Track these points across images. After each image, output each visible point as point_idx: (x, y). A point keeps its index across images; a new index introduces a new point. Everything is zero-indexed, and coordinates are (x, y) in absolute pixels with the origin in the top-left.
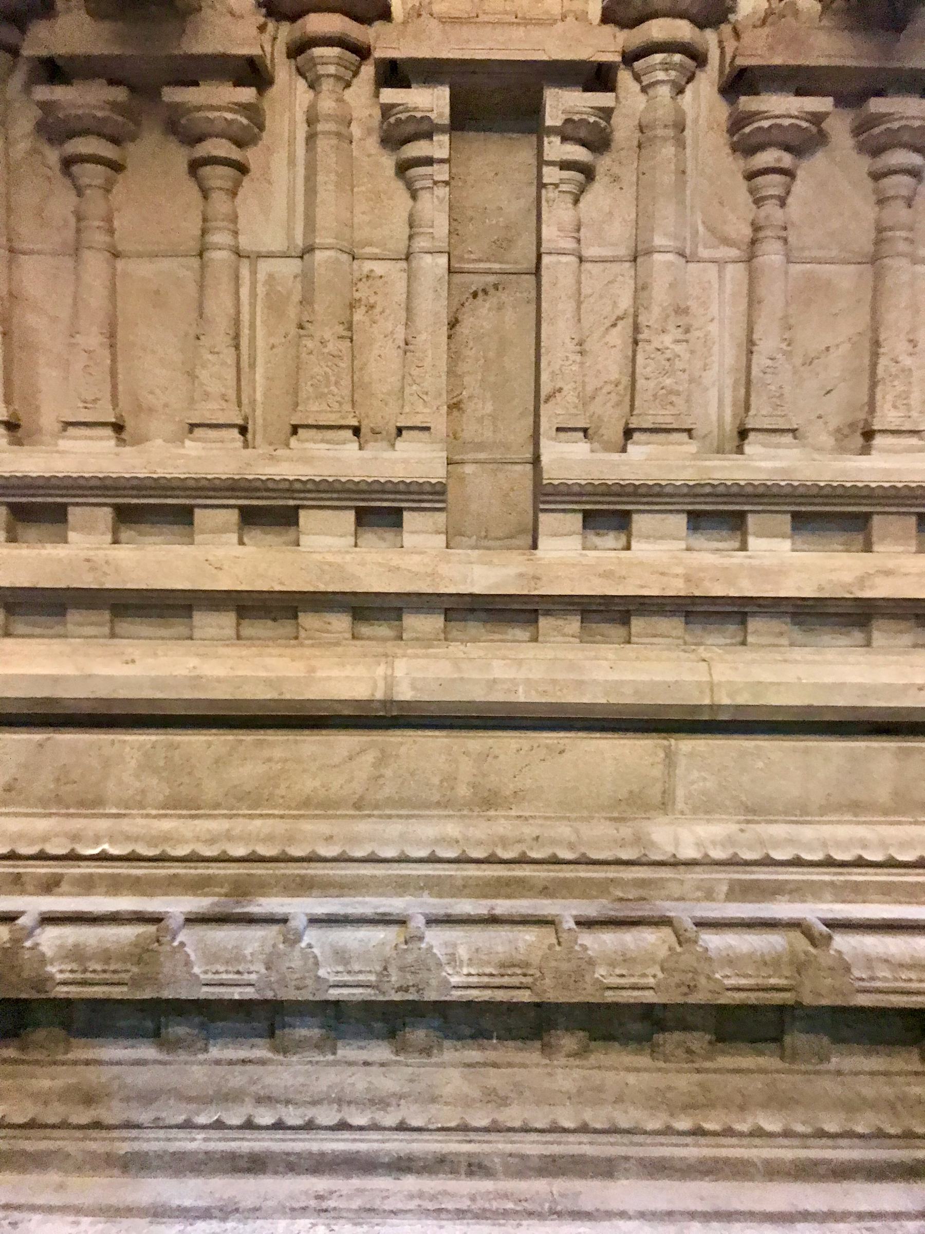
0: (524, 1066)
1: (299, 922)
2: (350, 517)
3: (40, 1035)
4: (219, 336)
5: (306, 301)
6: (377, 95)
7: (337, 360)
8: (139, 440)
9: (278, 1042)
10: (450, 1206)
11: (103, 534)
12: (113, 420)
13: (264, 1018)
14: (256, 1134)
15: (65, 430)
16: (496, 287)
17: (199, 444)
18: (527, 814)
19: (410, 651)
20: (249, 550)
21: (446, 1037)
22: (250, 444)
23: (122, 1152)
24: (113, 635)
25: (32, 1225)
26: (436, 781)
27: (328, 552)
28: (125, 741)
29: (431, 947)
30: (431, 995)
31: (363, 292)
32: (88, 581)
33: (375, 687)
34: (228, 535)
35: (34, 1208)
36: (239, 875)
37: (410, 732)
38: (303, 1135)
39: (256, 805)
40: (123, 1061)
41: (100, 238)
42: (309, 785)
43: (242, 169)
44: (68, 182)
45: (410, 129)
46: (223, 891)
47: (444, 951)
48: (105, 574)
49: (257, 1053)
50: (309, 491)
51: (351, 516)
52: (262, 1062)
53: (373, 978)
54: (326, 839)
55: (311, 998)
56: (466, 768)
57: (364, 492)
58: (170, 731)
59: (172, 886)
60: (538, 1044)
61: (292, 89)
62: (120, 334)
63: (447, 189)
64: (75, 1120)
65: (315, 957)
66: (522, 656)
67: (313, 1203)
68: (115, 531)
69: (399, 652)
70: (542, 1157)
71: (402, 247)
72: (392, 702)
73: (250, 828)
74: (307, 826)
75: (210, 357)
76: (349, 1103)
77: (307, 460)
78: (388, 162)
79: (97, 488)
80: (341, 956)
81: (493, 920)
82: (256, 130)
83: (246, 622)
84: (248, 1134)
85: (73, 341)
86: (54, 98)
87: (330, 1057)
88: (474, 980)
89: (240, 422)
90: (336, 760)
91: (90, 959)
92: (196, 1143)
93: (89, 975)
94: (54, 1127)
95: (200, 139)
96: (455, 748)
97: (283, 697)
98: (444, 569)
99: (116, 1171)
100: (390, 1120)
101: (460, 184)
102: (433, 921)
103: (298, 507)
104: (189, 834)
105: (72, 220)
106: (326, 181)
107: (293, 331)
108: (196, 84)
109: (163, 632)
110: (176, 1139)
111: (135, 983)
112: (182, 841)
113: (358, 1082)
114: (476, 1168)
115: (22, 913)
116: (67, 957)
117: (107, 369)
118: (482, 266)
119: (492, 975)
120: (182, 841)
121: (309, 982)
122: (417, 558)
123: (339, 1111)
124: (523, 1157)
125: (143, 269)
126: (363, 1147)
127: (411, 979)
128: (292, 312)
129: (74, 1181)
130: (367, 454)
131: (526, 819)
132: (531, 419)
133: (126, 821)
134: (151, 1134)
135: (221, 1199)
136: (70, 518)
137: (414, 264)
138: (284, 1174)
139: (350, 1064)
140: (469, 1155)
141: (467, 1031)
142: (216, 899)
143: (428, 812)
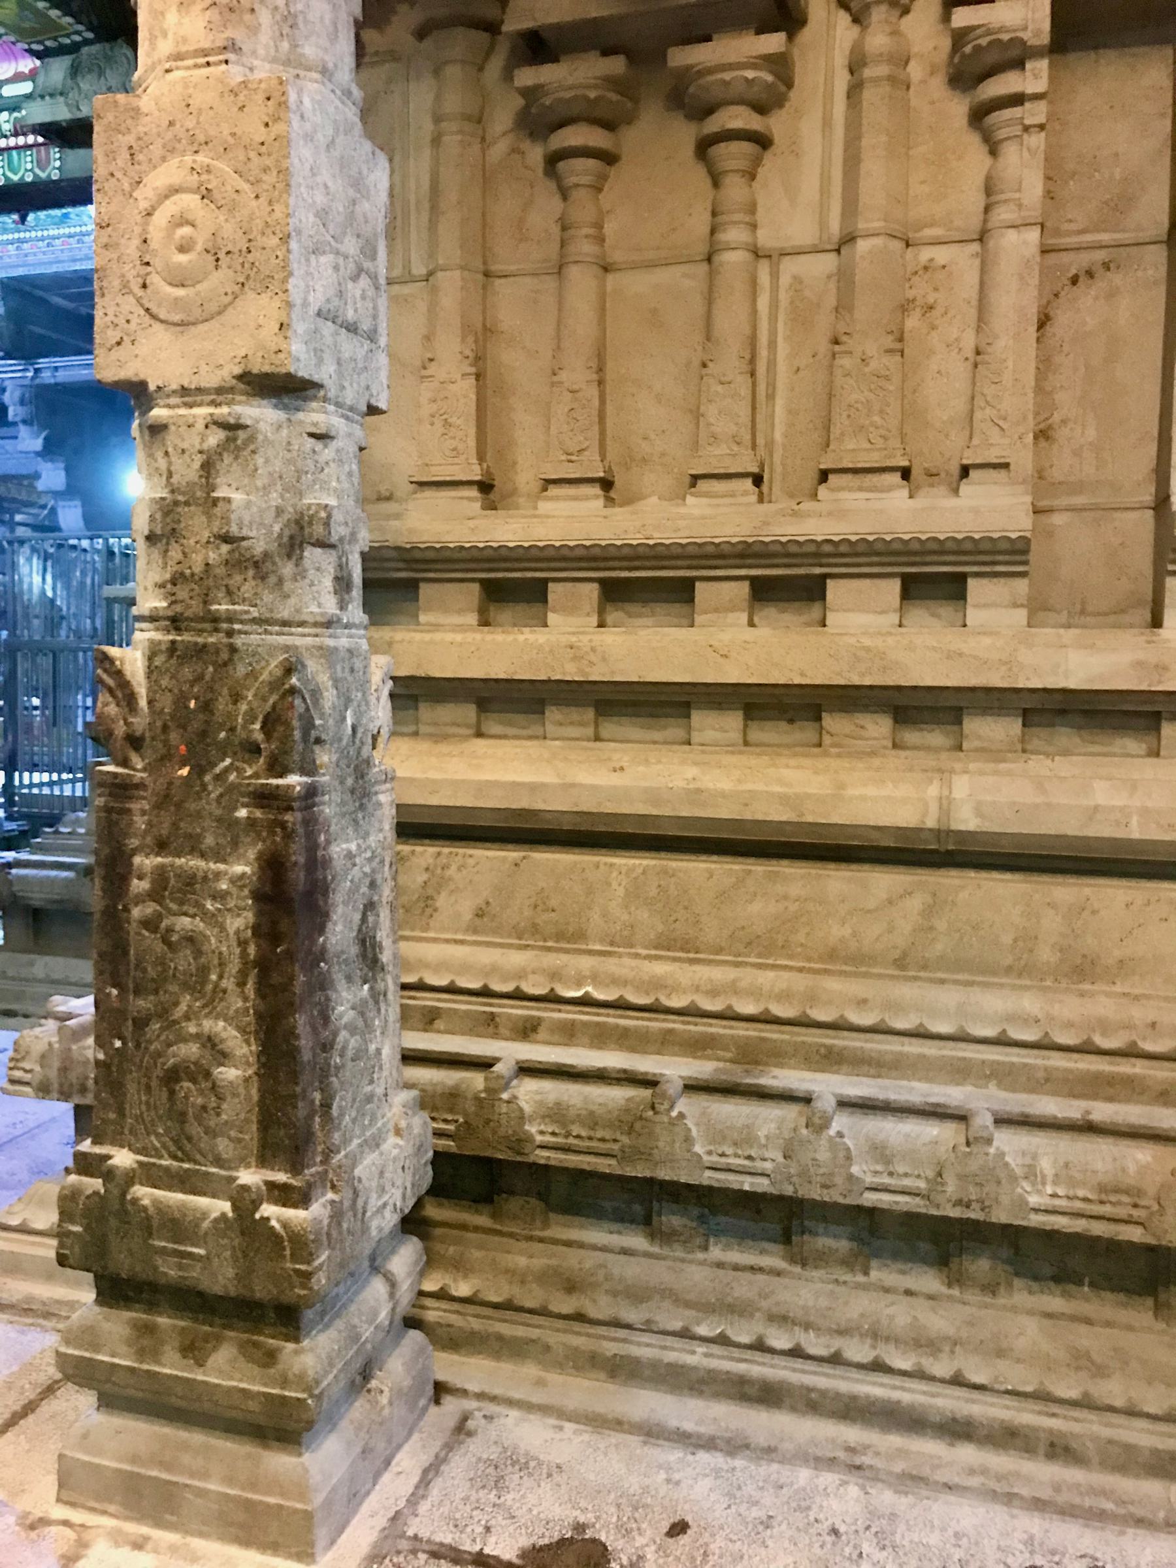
0: (1130, 1328)
1: (826, 1103)
2: (894, 587)
3: (514, 1204)
4: (730, 363)
5: (843, 307)
6: (946, 18)
7: (882, 382)
8: (628, 501)
9: (795, 1250)
10: (1025, 1492)
11: (588, 615)
12: (602, 474)
13: (781, 1218)
14: (767, 1358)
15: (546, 490)
16: (1106, 266)
17: (704, 500)
18: (1137, 991)
19: (972, 766)
20: (763, 633)
21: (1017, 1274)
22: (766, 499)
23: (609, 1354)
24: (597, 738)
25: (510, 1421)
26: (1007, 939)
27: (865, 634)
28: (612, 865)
29: (1003, 1154)
30: (1001, 1216)
31: (920, 290)
32: (570, 672)
33: (925, 814)
34: (737, 614)
35: (510, 1403)
36: (748, 1038)
37: (972, 874)
38: (827, 1369)
39: (768, 951)
40: (606, 1248)
41: (587, 248)
42: (837, 932)
43: (763, 141)
44: (553, 185)
45: (991, 58)
46: (729, 1055)
47: (1020, 1161)
48: (592, 663)
49: (766, 1261)
50: (843, 555)
51: (895, 586)
52: (779, 1273)
53: (922, 1184)
54: (858, 1003)
55: (841, 1200)
56: (1051, 924)
57: (915, 553)
58: (663, 855)
59: (665, 1043)
60: (1150, 1302)
61: (831, 26)
62: (610, 365)
63: (1043, 134)
64: (554, 1308)
65: (848, 1149)
66: (1136, 776)
67: (841, 1455)
68: (601, 612)
69: (958, 766)
70: (1155, 1452)
71: (975, 223)
72: (949, 832)
73: (760, 980)
74: (833, 985)
75: (720, 388)
76: (887, 1339)
77: (839, 514)
78: (958, 108)
79: (580, 559)
80: (881, 1152)
81: (1089, 1128)
82: (783, 88)
83: (754, 725)
84: (758, 1356)
85: (555, 379)
86: (542, 80)
87: (861, 1278)
88: (1061, 1203)
89: (755, 470)
90: (871, 904)
91: (573, 1123)
92: (697, 1357)
93: (571, 1141)
94: (531, 1311)
95: (709, 111)
96: (1037, 896)
97: (803, 820)
98: (1026, 656)
99: (602, 1375)
100: (941, 1368)
101: (1058, 127)
102: (1002, 1121)
103: (825, 577)
104: (686, 981)
105: (556, 230)
106: (872, 142)
107: (824, 347)
108: (708, 39)
109: (657, 735)
110: (673, 1349)
111: (623, 1157)
112: (675, 989)
113: (900, 1315)
114: (1059, 1450)
115: (498, 1060)
116: (549, 1116)
117: (595, 413)
118: (1089, 238)
119: (1086, 1200)
120: (675, 989)
121: (839, 1180)
122: (990, 640)
123: (874, 1347)
124: (1129, 1448)
125: (636, 284)
126: (906, 1398)
127: (973, 1193)
128: (824, 323)
129: (554, 1378)
130: (919, 502)
131: (1137, 998)
132: (1153, 449)
133: (612, 960)
134: (646, 1338)
135: (727, 1429)
136: (550, 597)
137: (991, 244)
138: (804, 1414)
139: (887, 1290)
140: (1051, 1431)
141: (1048, 1270)
142: (721, 1065)
143: (996, 980)
